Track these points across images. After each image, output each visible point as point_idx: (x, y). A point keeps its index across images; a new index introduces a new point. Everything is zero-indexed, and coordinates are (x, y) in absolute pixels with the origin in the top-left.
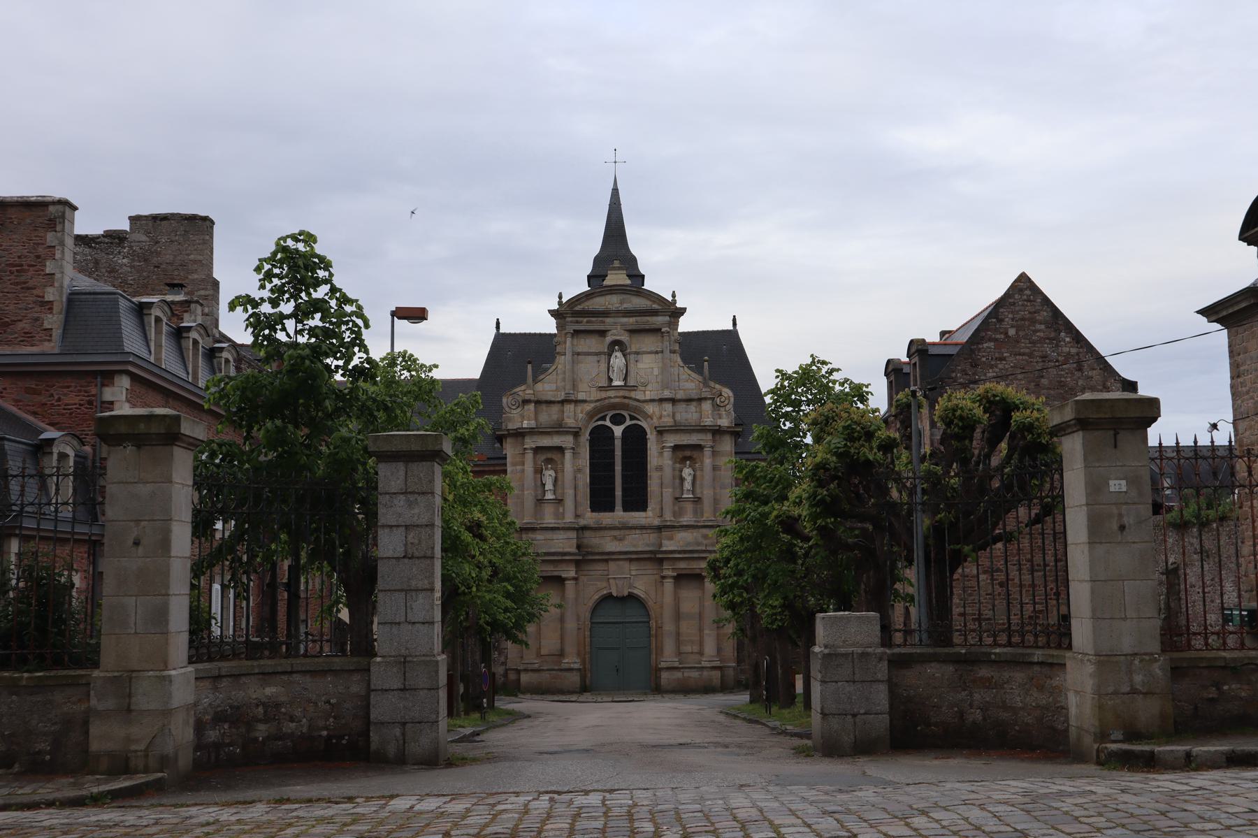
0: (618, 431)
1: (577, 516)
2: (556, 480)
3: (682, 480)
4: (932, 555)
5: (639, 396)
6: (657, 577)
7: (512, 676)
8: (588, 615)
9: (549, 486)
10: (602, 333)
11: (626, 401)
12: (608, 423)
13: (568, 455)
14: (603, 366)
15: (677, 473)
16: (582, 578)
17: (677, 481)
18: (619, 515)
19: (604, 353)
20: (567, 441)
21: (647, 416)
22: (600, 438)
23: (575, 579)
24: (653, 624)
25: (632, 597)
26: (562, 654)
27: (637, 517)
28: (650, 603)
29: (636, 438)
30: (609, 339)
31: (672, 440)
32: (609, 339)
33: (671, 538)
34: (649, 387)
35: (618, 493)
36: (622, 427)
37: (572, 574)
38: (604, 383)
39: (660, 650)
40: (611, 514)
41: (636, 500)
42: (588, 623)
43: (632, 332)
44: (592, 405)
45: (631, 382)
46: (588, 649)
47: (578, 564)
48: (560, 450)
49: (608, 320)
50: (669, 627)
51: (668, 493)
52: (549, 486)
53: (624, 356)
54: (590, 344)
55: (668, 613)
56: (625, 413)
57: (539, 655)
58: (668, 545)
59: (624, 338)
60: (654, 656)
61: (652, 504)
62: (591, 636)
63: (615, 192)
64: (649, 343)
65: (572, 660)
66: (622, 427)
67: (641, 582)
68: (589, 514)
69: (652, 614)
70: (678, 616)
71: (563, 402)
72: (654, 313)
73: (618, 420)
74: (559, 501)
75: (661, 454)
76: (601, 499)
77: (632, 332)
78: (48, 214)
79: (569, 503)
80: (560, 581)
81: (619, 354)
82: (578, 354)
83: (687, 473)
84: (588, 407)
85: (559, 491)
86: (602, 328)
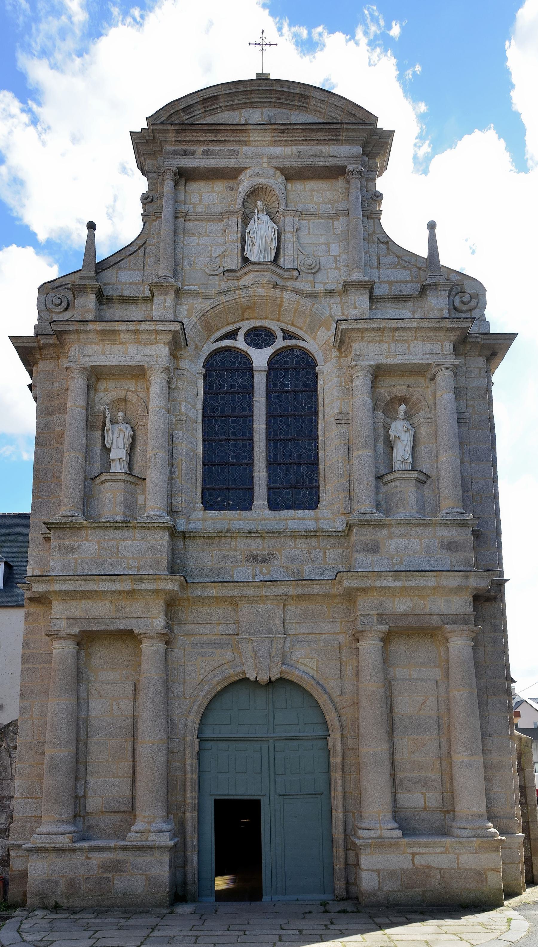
0: (260, 358)
3: (389, 444)
4: (268, 96)
9: (118, 452)
10: (230, 175)
12: (240, 343)
14: (234, 237)
15: (381, 431)
17: (381, 446)
18: (261, 514)
22: (225, 373)
24: (335, 740)
25: (283, 681)
29: (295, 373)
30: (245, 183)
32: (245, 183)
33: (374, 548)
34: (319, 276)
36: (269, 351)
40: (244, 513)
41: (296, 486)
45: (287, 261)
49: (245, 150)
50: (373, 747)
51: (363, 460)
52: (118, 452)
55: (370, 717)
61: (330, 491)
62: (200, 771)
64: (316, 195)
66: (269, 351)
68: (199, 513)
73: (260, 337)
76: (224, 486)
77: (291, 175)
78: (460, 140)
79: (155, 478)
83: (399, 429)
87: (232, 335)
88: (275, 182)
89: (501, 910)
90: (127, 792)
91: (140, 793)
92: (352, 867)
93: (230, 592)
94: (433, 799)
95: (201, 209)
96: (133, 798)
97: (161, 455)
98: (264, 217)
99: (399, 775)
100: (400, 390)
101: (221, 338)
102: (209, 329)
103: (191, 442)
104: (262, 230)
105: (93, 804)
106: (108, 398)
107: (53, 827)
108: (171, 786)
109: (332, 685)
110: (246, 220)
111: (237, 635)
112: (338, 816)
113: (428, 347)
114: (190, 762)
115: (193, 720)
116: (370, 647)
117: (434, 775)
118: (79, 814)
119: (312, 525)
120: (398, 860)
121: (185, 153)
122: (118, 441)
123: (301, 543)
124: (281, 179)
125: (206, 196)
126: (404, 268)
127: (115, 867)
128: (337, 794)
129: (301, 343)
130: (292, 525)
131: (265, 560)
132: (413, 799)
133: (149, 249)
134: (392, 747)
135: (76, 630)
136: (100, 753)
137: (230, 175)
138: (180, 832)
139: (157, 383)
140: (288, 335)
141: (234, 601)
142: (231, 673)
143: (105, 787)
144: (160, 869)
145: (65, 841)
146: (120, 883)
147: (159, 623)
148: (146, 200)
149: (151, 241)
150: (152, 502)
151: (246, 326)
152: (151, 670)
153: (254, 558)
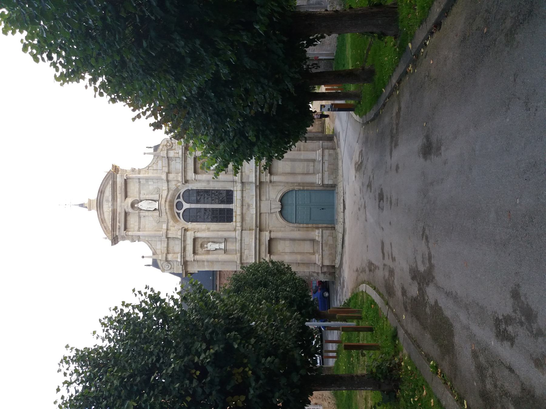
0: (186, 206)
2: (214, 242)
5: (165, 193)
6: (270, 185)
7: (325, 270)
8: (291, 225)
9: (217, 246)
11: (168, 200)
12: (181, 212)
13: (198, 235)
14: (147, 213)
16: (270, 228)
18: (236, 206)
19: (139, 213)
20: (190, 236)
21: (177, 189)
22: (192, 216)
23: (270, 232)
24: (296, 188)
25: (281, 200)
26: (313, 241)
27: (237, 196)
28: (285, 190)
29: (189, 195)
30: (130, 210)
31: (191, 175)
32: (130, 210)
35: (222, 206)
36: (184, 203)
37: (267, 233)
38: (157, 213)
39: (312, 184)
42: (296, 225)
43: (126, 196)
44: (170, 220)
45: (156, 197)
46: (310, 226)
47: (261, 230)
48: (195, 240)
49: (118, 211)
52: (217, 246)
53: (141, 201)
54: (133, 221)
56: (176, 201)
57: (314, 253)
58: (253, 179)
59: (129, 200)
60: (315, 188)
61: (229, 187)
64: (133, 188)
65: (316, 234)
66: (184, 203)
67: (273, 195)
69: (291, 188)
70: (293, 174)
72: (114, 184)
73: (179, 206)
74: (226, 240)
75: (200, 181)
76: (225, 216)
77: (126, 196)
80: (271, 240)
82: (139, 228)
84: (171, 223)
85: (220, 240)
86: (123, 214)
87: (178, 214)
88: (129, 200)
89: (253, 198)
90: (308, 242)
98: (140, 204)
99: (306, 172)
101: (179, 217)
102: (177, 221)
103: (214, 226)
104: (143, 205)
117: (306, 163)
121: (119, 229)
126: (157, 162)
129: (181, 194)
133: (150, 239)
134: (299, 174)
135: (268, 255)
137: (126, 214)
140: (179, 197)
142: (278, 215)
148: (133, 241)
149: (147, 239)
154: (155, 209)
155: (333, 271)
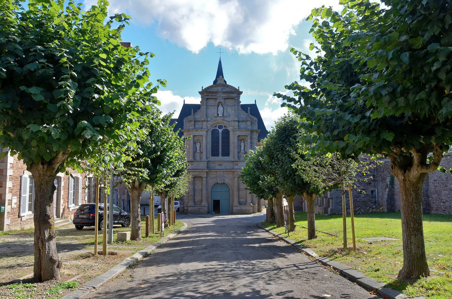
0: (220, 131)
1: (207, 158)
3: (241, 146)
9: (198, 148)
12: (217, 128)
14: (216, 110)
18: (220, 158)
22: (214, 133)
24: (231, 192)
27: (226, 158)
29: (226, 133)
30: (218, 101)
33: (237, 165)
35: (220, 150)
36: (222, 130)
38: (216, 115)
41: (226, 153)
45: (225, 115)
51: (236, 150)
52: (198, 148)
55: (236, 189)
59: (222, 101)
61: (231, 154)
63: (220, 62)
64: (230, 102)
66: (222, 130)
71: (203, 121)
73: (220, 127)
76: (215, 153)
79: (204, 153)
81: (221, 106)
83: (242, 144)
87: (216, 127)
88: (222, 101)
91: (203, 199)
92: (232, 209)
93: (216, 170)
94: (244, 200)
95: (210, 104)
96: (202, 200)
97: (205, 150)
100: (242, 138)
103: (210, 146)
104: (221, 108)
105: (196, 200)
106: (196, 139)
107: (191, 203)
108: (207, 198)
109: (231, 184)
110: (218, 107)
111: (207, 99)
112: (231, 202)
113: (247, 132)
114: (210, 195)
115: (210, 189)
116: (236, 179)
118: (194, 202)
119: (228, 160)
120: (239, 208)
121: (208, 96)
122: (198, 146)
123: (227, 163)
124: (224, 100)
125: (211, 102)
127: (200, 209)
128: (231, 199)
130: (225, 160)
131: (221, 165)
132: (242, 200)
136: (197, 194)
138: (208, 204)
139: (204, 138)
140: (225, 127)
141: (216, 172)
142: (216, 182)
143: (198, 198)
144: (206, 209)
145: (193, 205)
146: (201, 210)
147: (205, 175)
150: (204, 158)
151: (218, 125)
152: (204, 182)
153: (219, 165)
154: (218, 114)
155: (185, 212)
